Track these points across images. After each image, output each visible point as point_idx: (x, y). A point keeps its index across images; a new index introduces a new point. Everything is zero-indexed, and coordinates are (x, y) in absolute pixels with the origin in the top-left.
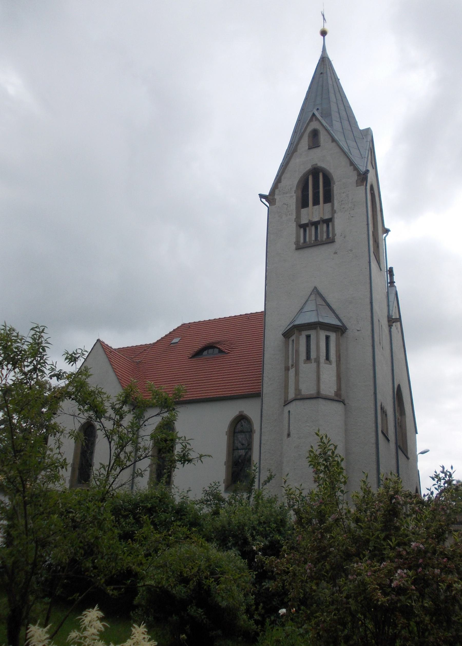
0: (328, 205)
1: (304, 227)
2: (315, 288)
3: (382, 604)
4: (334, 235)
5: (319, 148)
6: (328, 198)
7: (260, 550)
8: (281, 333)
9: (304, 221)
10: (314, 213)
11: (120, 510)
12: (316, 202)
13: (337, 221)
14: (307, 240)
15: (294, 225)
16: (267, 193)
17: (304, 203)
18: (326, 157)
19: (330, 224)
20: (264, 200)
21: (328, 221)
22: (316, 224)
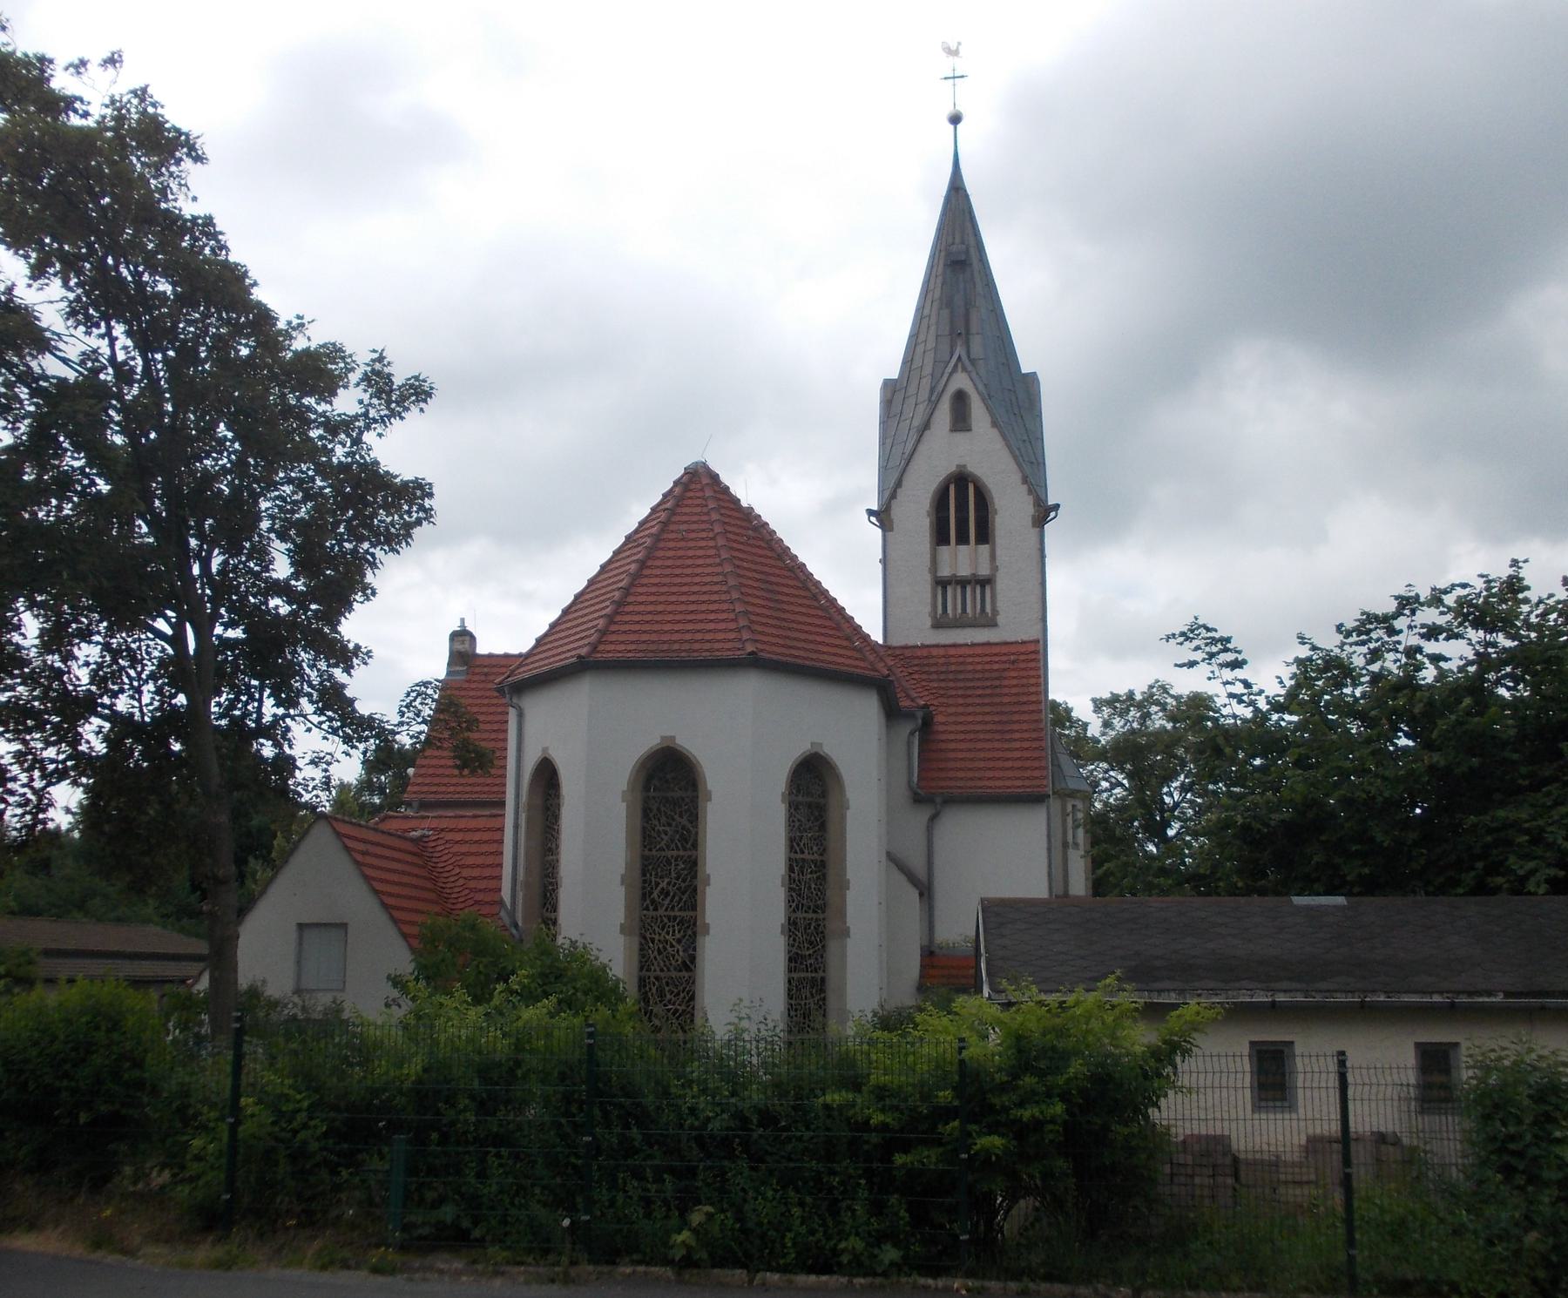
0: (984, 549)
1: (941, 584)
2: (1094, 700)
3: (153, 718)
4: (995, 612)
5: (968, 434)
6: (984, 536)
7: (82, 494)
8: (712, 881)
9: (945, 572)
10: (962, 560)
11: (300, 1225)
12: (963, 539)
13: (1001, 583)
14: (969, 610)
15: (928, 577)
16: (875, 507)
17: (941, 537)
18: (982, 452)
19: (988, 589)
20: (873, 519)
21: (985, 582)
22: (963, 583)
